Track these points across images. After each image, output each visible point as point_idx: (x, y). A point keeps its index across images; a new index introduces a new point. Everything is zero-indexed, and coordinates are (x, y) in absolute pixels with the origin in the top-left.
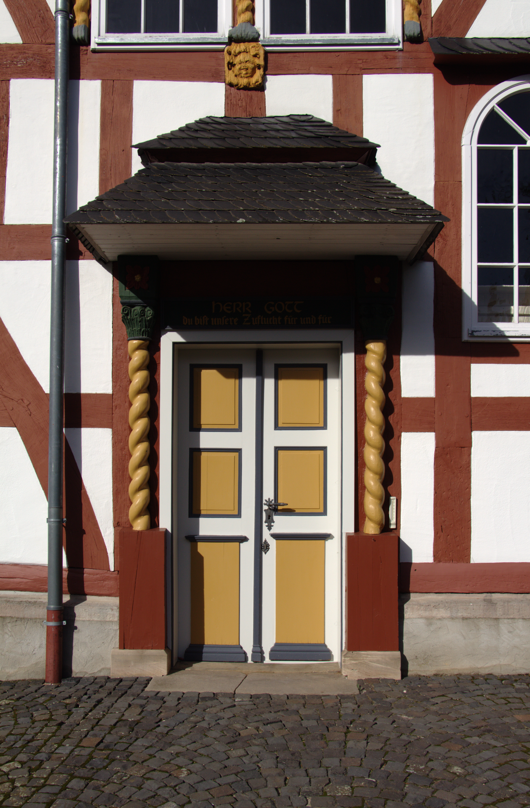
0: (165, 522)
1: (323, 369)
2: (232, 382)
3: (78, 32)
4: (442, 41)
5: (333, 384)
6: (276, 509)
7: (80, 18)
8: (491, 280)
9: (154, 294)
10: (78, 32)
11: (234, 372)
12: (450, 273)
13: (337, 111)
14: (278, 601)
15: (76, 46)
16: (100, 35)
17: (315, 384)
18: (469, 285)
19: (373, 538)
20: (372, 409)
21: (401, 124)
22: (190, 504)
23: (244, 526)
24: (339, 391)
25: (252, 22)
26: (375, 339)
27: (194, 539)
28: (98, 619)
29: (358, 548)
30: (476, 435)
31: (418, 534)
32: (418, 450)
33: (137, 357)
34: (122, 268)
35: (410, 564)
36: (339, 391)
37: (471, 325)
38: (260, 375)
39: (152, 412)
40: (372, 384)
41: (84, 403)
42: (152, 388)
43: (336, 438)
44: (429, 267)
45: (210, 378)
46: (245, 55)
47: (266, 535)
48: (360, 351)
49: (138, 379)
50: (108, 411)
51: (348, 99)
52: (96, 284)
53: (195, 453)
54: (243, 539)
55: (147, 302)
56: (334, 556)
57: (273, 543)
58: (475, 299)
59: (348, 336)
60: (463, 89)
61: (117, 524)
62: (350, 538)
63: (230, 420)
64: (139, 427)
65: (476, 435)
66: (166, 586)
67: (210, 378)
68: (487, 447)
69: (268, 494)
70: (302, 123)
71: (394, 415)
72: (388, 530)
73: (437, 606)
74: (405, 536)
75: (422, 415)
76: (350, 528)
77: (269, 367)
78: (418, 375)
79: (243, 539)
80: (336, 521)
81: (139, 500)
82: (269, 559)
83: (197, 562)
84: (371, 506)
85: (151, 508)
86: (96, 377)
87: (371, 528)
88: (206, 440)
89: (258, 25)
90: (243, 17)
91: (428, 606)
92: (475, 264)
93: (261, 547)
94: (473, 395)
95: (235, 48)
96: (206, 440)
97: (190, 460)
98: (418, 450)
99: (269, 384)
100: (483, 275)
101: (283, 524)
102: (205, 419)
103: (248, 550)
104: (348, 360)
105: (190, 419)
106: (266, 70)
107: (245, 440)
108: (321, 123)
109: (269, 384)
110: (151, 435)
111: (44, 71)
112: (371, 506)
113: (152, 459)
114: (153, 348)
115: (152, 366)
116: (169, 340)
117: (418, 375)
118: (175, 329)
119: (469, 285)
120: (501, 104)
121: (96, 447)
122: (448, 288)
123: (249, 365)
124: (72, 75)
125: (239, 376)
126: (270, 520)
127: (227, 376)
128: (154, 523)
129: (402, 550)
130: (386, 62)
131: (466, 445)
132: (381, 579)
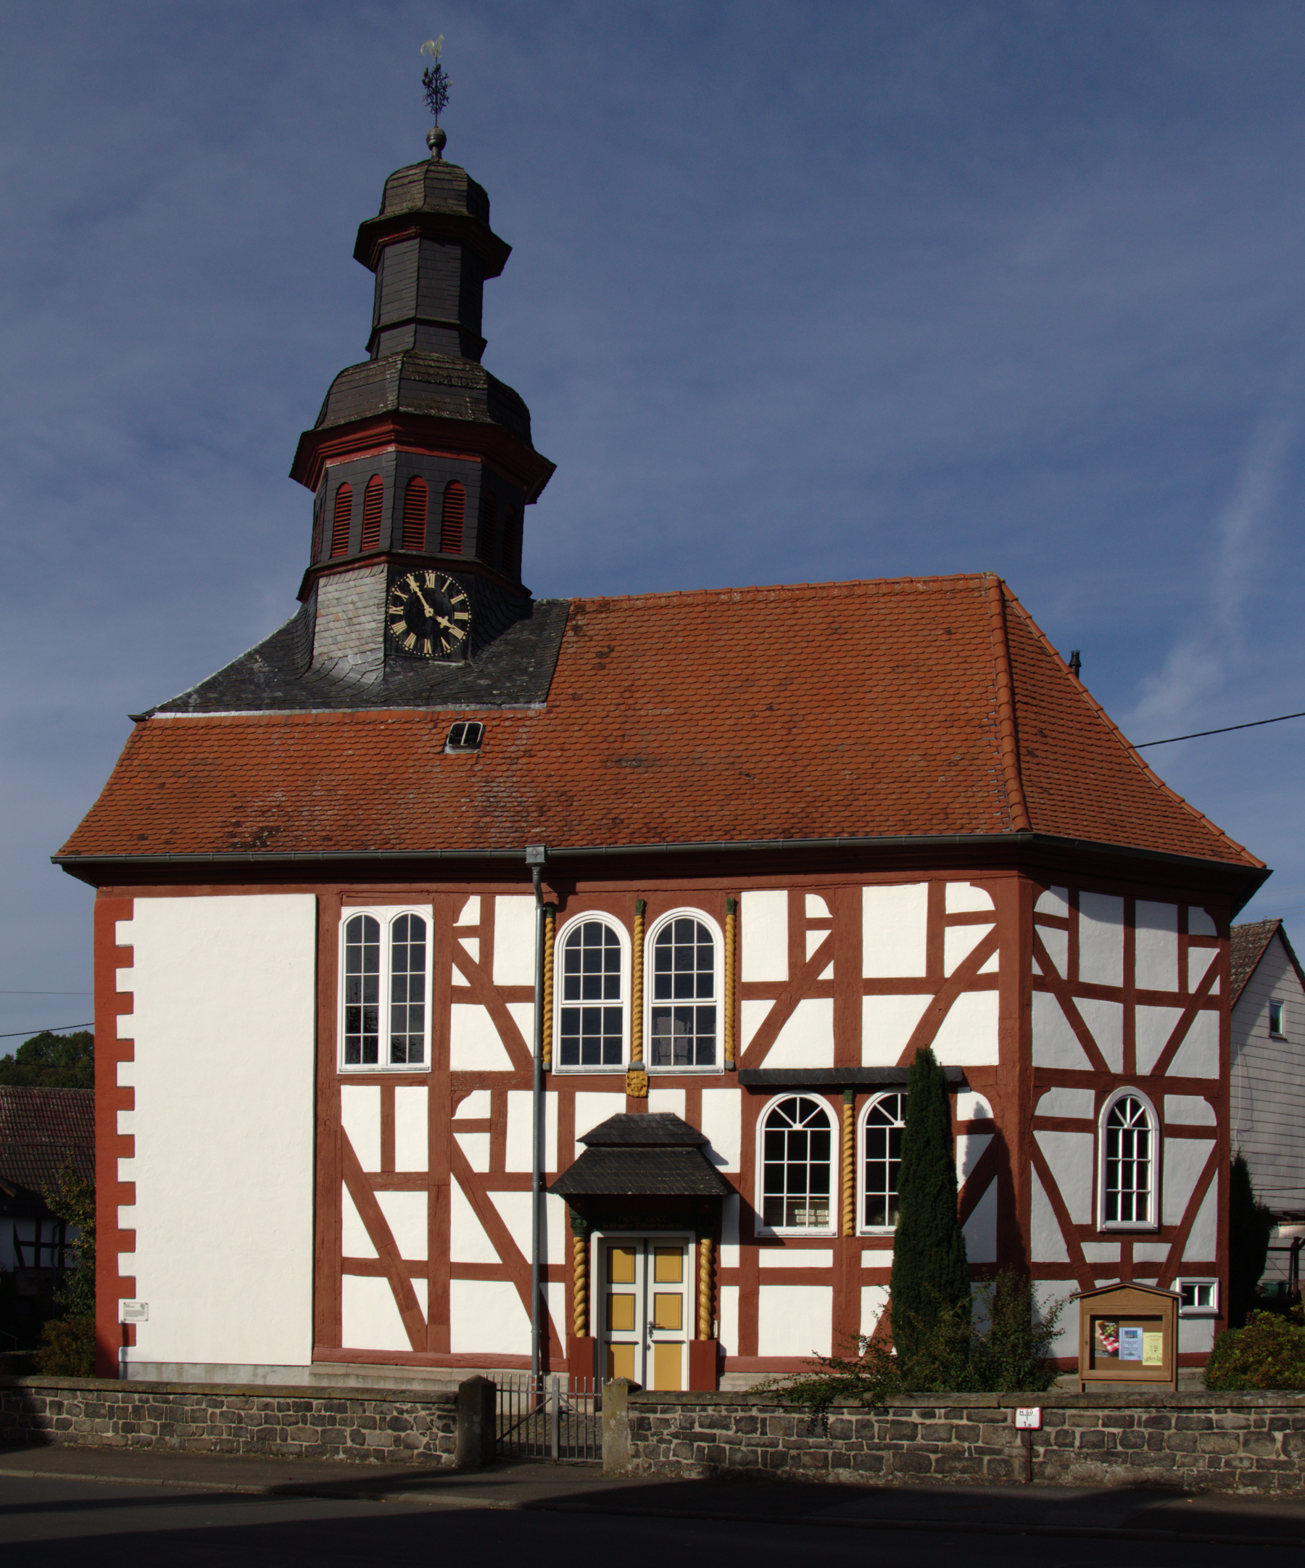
0: (593, 1332)
1: (681, 1251)
2: (630, 1257)
3: (546, 1067)
4: (746, 1072)
5: (685, 1257)
6: (654, 1327)
7: (546, 1058)
8: (772, 1207)
9: (588, 1212)
10: (546, 1067)
11: (631, 1251)
12: (748, 1200)
13: (688, 1111)
14: (655, 1358)
15: (544, 1074)
16: (557, 1066)
17: (677, 1258)
18: (759, 1208)
19: (703, 1342)
20: (704, 1274)
21: (722, 1120)
22: (607, 1323)
23: (637, 1336)
24: (689, 1260)
25: (641, 1059)
26: (706, 1237)
27: (609, 1343)
28: (559, 1380)
29: (694, 1346)
30: (762, 1288)
31: (730, 1341)
32: (730, 1297)
33: (579, 1246)
34: (570, 1200)
35: (725, 1357)
36: (689, 1260)
37: (759, 1228)
38: (646, 1253)
39: (586, 1275)
40: (704, 1261)
41: (550, 1270)
42: (586, 1262)
43: (687, 1288)
44: (737, 1197)
45: (618, 1255)
46: (637, 1079)
47: (649, 1341)
48: (698, 1243)
49: (579, 1257)
50: (563, 1273)
51: (694, 1105)
52: (556, 1206)
53: (610, 1295)
54: (636, 1343)
55: (583, 1217)
56: (685, 1349)
57: (652, 1345)
58: (762, 1215)
59: (692, 1235)
60: (756, 1098)
61: (568, 1334)
62: (691, 1342)
63: (630, 1278)
64: (580, 1283)
65: (762, 1288)
66: (594, 1357)
67: (618, 1255)
68: (767, 1294)
69: (650, 1318)
70: (669, 1119)
71: (714, 1277)
72: (714, 1340)
73: (738, 1378)
74: (722, 1342)
75: (732, 1277)
76: (693, 1338)
77: (651, 1248)
78: (730, 1255)
79: (636, 1343)
80: (687, 1334)
81: (580, 1321)
82: (651, 1354)
83: (611, 1356)
84: (703, 1325)
85: (586, 1326)
86: (556, 1255)
87: (703, 1337)
88: (616, 1288)
89: (645, 1061)
90: (636, 1058)
91: (733, 1378)
92: (763, 1195)
93: (646, 1348)
94: (761, 1265)
95: (633, 1074)
96: (616, 1288)
97: (607, 1300)
98: (730, 1297)
99: (651, 1258)
100: (767, 1201)
101: (658, 1335)
102: (615, 1277)
103: (639, 1349)
104: (692, 1247)
105: (607, 1277)
106: (648, 1087)
107: (637, 1289)
108: (679, 1119)
109: (651, 1258)
110: (586, 1287)
111: (525, 1086)
112: (703, 1325)
113: (586, 1300)
114: (587, 1240)
115: (586, 1250)
116: (595, 1236)
117: (730, 1255)
118: (598, 1230)
119: (759, 1208)
120: (779, 1106)
121: (556, 1293)
122: (747, 1209)
123: (640, 1248)
124: (543, 1088)
125: (635, 1254)
126: (651, 1332)
127: (627, 1253)
128: (587, 1333)
129: (719, 1349)
130: (715, 1082)
131: (756, 1293)
132: (708, 1358)
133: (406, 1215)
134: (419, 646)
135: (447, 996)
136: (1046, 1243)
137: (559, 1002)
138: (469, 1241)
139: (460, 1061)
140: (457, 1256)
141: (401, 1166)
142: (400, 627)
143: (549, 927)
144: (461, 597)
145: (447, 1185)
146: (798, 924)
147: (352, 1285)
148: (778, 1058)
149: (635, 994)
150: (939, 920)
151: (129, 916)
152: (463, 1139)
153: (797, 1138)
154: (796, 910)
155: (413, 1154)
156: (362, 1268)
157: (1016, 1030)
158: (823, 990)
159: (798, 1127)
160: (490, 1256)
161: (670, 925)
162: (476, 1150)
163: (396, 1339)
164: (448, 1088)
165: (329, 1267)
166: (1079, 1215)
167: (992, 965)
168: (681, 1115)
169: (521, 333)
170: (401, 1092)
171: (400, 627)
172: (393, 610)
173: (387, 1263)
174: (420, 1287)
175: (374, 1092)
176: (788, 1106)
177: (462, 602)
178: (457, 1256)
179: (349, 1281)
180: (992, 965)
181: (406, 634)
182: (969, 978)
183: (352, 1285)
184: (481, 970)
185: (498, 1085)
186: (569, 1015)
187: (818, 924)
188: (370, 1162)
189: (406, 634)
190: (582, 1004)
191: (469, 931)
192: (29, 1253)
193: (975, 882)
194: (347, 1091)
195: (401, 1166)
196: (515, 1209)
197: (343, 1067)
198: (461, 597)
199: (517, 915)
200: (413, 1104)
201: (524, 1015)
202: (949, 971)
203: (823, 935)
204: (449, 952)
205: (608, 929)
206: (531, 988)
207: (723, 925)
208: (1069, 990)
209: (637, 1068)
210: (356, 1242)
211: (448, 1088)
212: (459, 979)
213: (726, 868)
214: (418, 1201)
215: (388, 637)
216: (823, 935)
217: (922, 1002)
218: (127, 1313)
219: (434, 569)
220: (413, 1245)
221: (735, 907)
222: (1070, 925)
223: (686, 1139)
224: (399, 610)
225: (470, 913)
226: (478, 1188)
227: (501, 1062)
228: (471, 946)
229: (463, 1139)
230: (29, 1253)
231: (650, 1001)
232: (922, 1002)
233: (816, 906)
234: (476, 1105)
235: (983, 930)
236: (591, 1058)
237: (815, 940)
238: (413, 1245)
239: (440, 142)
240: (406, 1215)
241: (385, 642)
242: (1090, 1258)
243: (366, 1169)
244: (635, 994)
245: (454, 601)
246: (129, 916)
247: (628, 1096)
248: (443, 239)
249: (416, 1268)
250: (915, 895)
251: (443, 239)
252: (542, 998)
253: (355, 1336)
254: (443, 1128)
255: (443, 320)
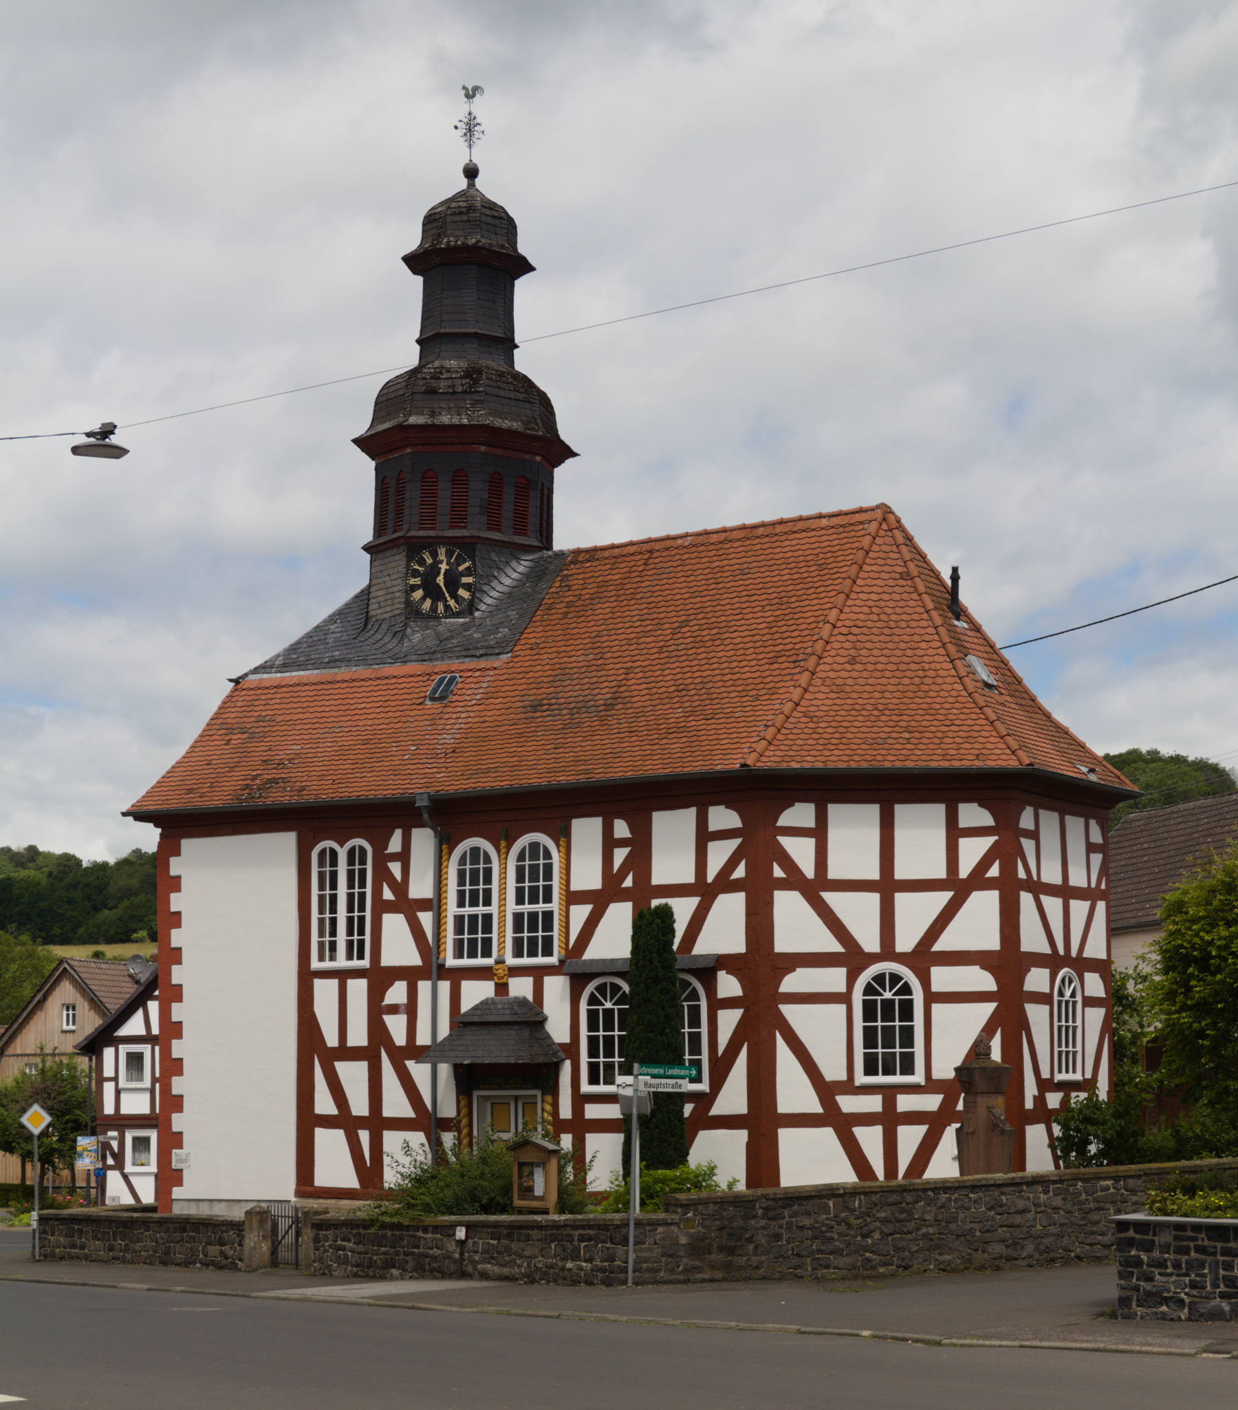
70: (522, 1002)
95: (498, 967)
134: (434, 608)
135: (382, 906)
137: (452, 908)
140: (387, 1112)
141: (352, 1042)
142: (418, 594)
143: (445, 851)
144: (467, 564)
145: (380, 1056)
148: (593, 952)
149: (505, 904)
150: (704, 837)
151: (178, 854)
152: (389, 1019)
154: (608, 830)
155: (358, 1036)
157: (759, 923)
159: (608, 1005)
160: (408, 1112)
161: (524, 848)
162: (396, 1026)
163: (350, 1180)
165: (308, 1121)
167: (740, 872)
168: (530, 998)
171: (418, 594)
172: (412, 581)
173: (344, 1120)
174: (364, 1136)
176: (601, 989)
177: (468, 569)
178: (387, 1112)
179: (319, 1132)
180: (740, 872)
181: (423, 599)
182: (725, 883)
184: (401, 888)
185: (410, 975)
186: (459, 920)
187: (622, 843)
188: (332, 1040)
189: (423, 599)
190: (527, 908)
195: (352, 1042)
196: (420, 1072)
197: (315, 964)
198: (467, 564)
202: (710, 878)
203: (626, 850)
204: (382, 875)
205: (545, 847)
206: (430, 901)
207: (558, 846)
208: (814, 889)
209: (500, 961)
211: (380, 978)
215: (408, 603)
216: (626, 850)
217: (945, 896)
218: (177, 1161)
219: (444, 544)
221: (567, 833)
224: (417, 581)
225: (395, 845)
226: (400, 1056)
227: (415, 959)
229: (389, 1019)
232: (945, 896)
234: (397, 993)
235: (734, 843)
237: (620, 855)
239: (471, 172)
241: (405, 608)
242: (363, 1042)
243: (329, 1045)
244: (505, 904)
245: (461, 568)
246: (178, 854)
247: (496, 985)
248: (469, 258)
250: (688, 816)
251: (469, 258)
252: (440, 907)
253: (323, 1178)
254: (377, 1010)
255: (456, 330)
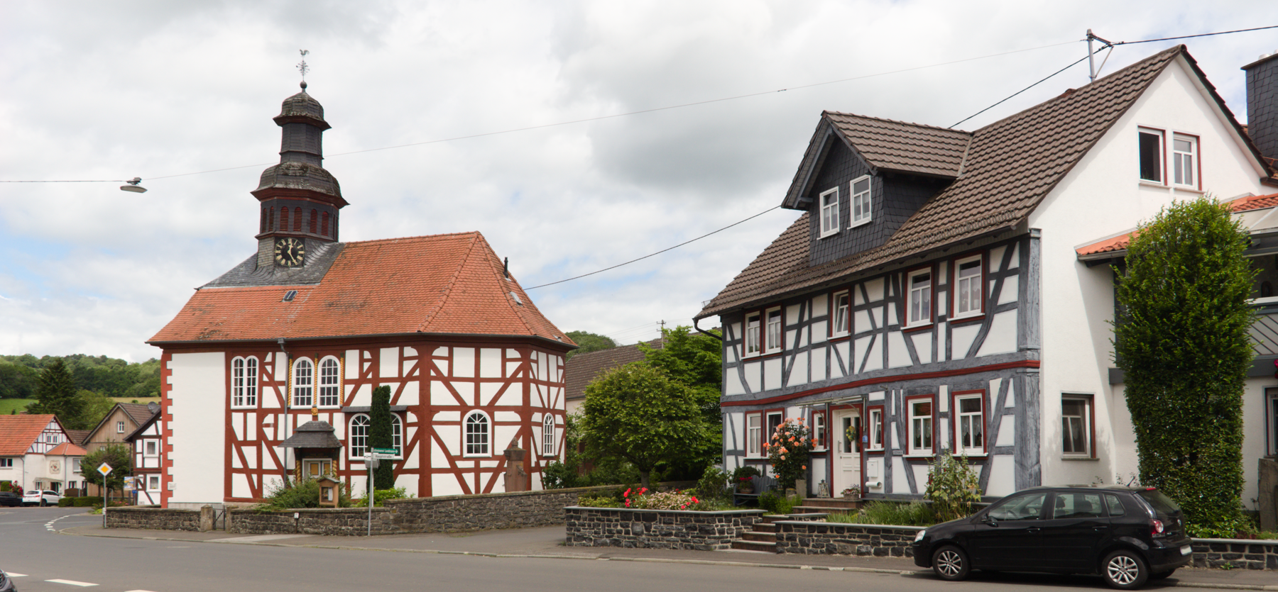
70: (324, 423)
133: (250, 452)
135: (262, 384)
136: (438, 459)
137: (294, 385)
138: (268, 463)
139: (265, 406)
141: (249, 438)
142: (279, 257)
146: (362, 361)
147: (235, 476)
149: (316, 384)
150: (402, 359)
152: (265, 429)
153: (477, 426)
154: (361, 355)
155: (252, 436)
156: (238, 471)
157: (425, 393)
158: (368, 381)
162: (269, 433)
164: (262, 413)
165: (229, 471)
166: (455, 451)
167: (417, 373)
169: (336, 153)
170: (249, 415)
173: (246, 470)
174: (255, 477)
175: (241, 414)
176: (358, 418)
180: (417, 373)
182: (410, 377)
183: (235, 476)
184: (271, 377)
185: (275, 412)
187: (367, 360)
188: (240, 437)
191: (268, 364)
192: (469, 478)
193: (413, 346)
194: (234, 414)
196: (279, 451)
197: (233, 407)
199: (281, 358)
200: (252, 417)
201: (282, 389)
204: (263, 370)
210: (236, 463)
211: (262, 413)
212: (265, 379)
213: (338, 345)
214: (254, 449)
215: (275, 261)
220: (252, 464)
222: (450, 359)
223: (328, 431)
225: (269, 358)
226: (270, 445)
228: (269, 368)
229: (265, 429)
230: (469, 478)
231: (320, 385)
233: (367, 355)
234: (269, 419)
236: (329, 403)
237: (366, 365)
238: (252, 464)
239: (304, 86)
240: (250, 452)
244: (316, 384)
248: (303, 122)
249: (253, 471)
250: (395, 351)
251: (303, 122)
253: (236, 493)
254: (260, 426)
